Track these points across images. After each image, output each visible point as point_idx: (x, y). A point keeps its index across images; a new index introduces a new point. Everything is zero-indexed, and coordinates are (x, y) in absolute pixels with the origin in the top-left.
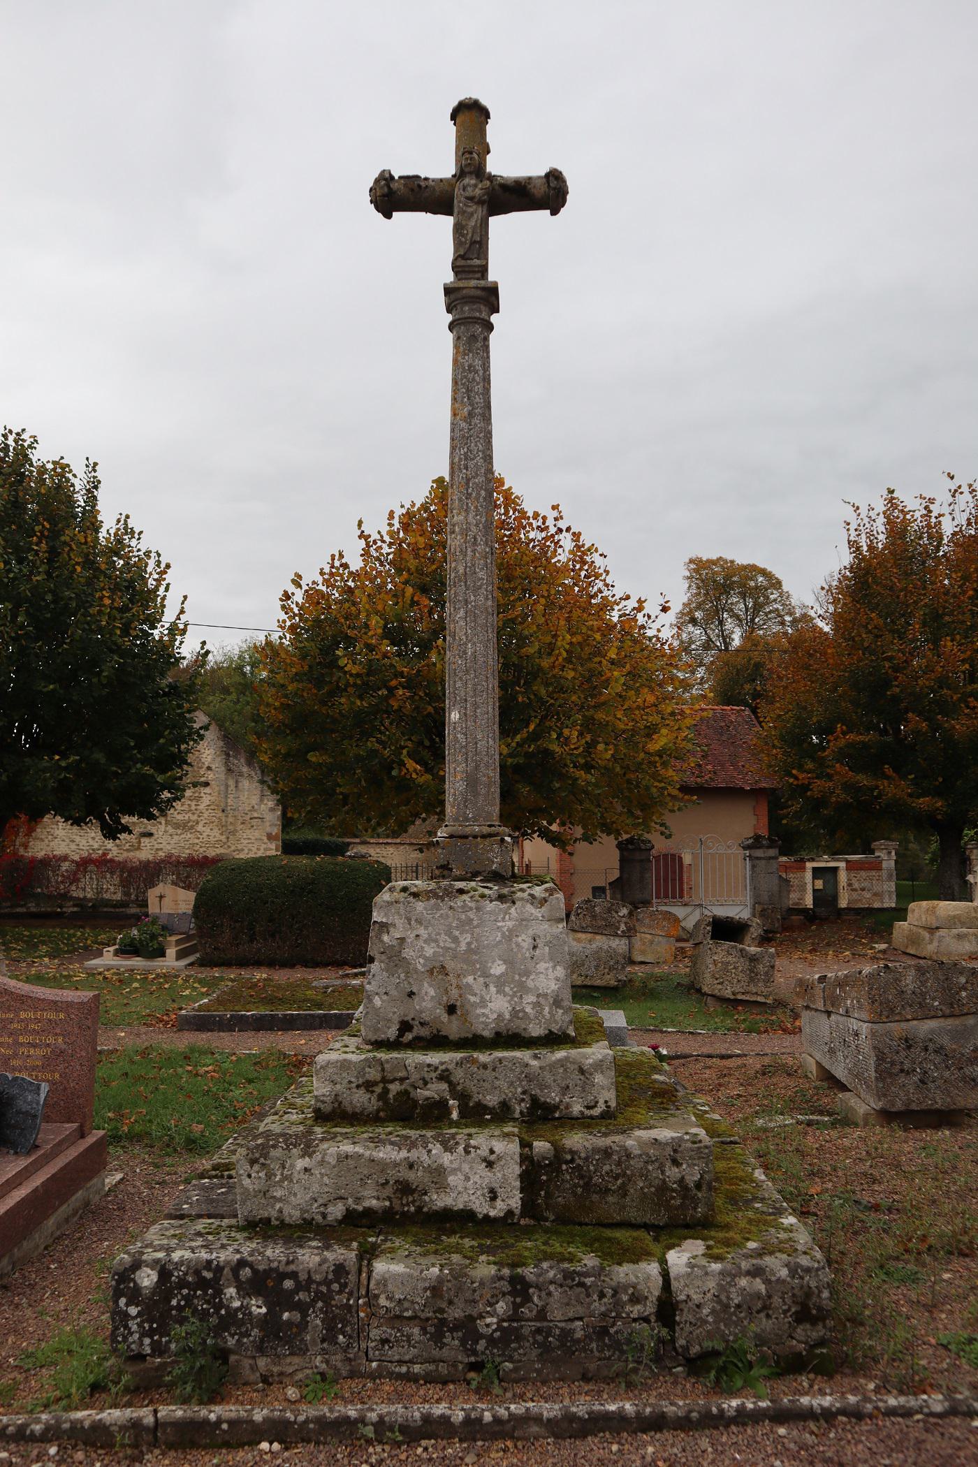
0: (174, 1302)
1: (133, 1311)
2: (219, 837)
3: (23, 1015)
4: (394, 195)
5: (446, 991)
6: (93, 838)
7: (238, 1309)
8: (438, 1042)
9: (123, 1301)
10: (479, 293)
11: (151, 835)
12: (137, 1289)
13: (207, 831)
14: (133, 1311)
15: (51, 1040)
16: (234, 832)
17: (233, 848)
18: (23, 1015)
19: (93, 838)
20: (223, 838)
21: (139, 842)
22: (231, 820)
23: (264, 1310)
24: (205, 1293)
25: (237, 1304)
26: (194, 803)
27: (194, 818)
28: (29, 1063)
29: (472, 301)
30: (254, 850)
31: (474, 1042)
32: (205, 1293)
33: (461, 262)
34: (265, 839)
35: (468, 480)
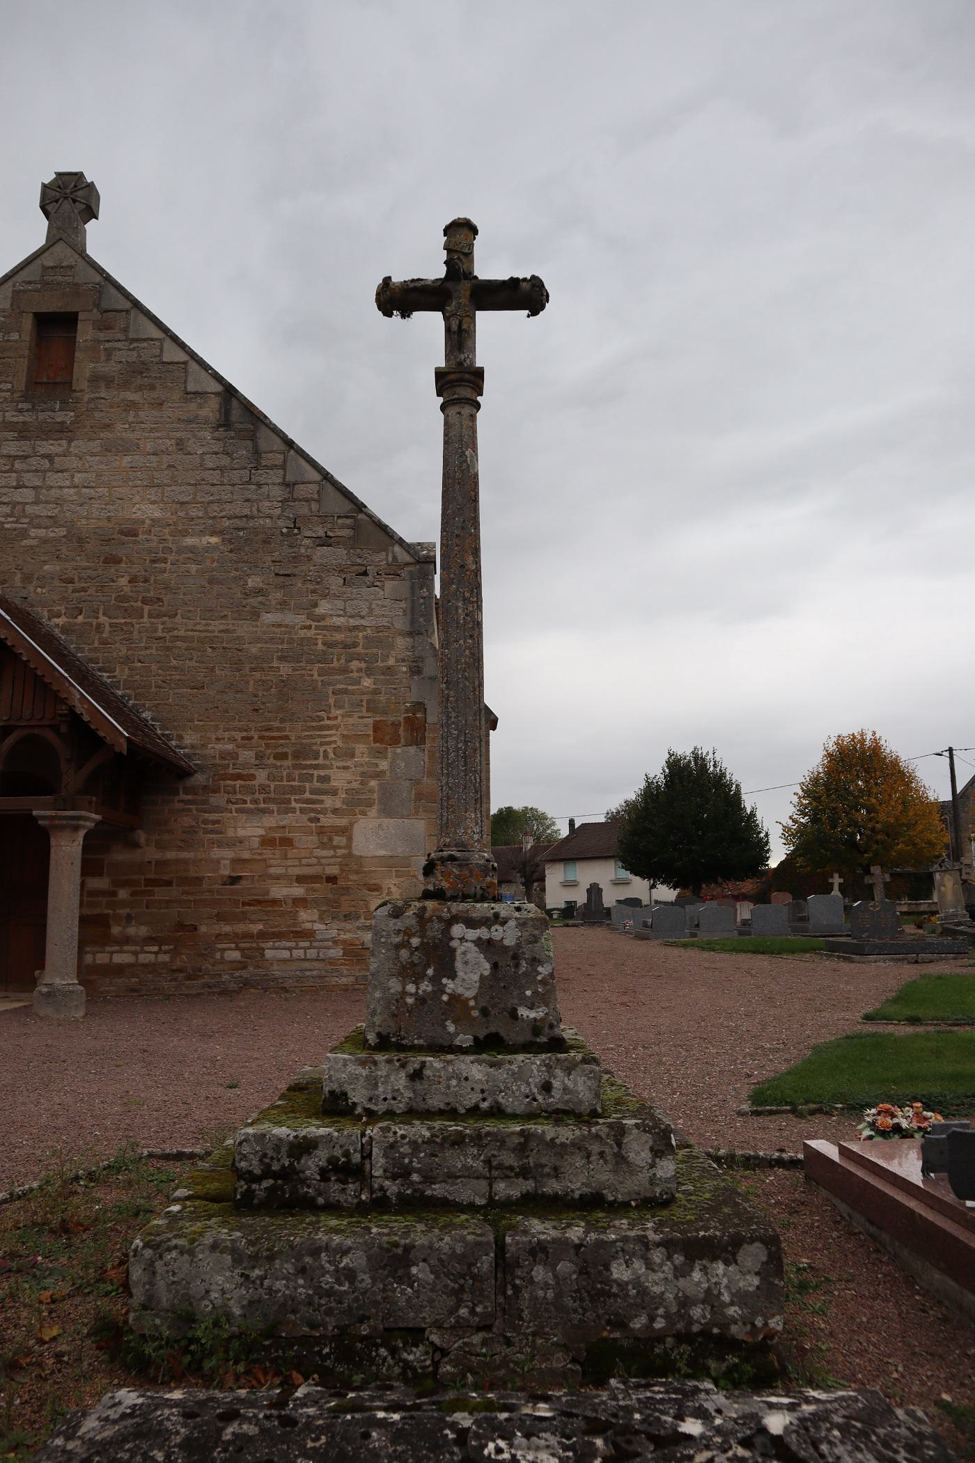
29: (460, 383)
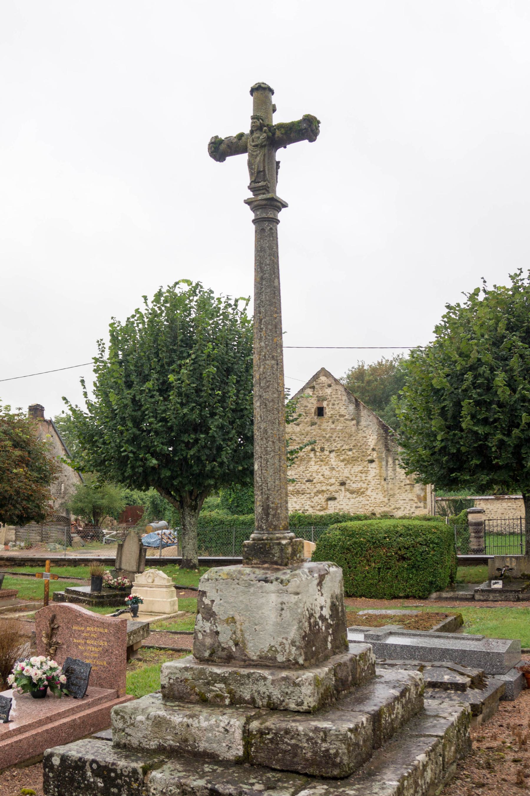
0: (67, 774)
1: (51, 775)
2: (383, 499)
3: (88, 629)
4: (220, 149)
5: (234, 633)
6: (296, 502)
7: (92, 782)
8: (229, 659)
9: (47, 770)
10: (264, 202)
11: (334, 499)
12: (52, 765)
13: (374, 495)
14: (51, 775)
15: (102, 643)
16: (393, 495)
17: (393, 507)
18: (88, 629)
19: (296, 502)
20: (386, 500)
21: (327, 504)
22: (390, 486)
23: (102, 785)
24: (79, 773)
25: (92, 780)
26: (364, 475)
27: (365, 486)
28: (92, 655)
29: (266, 207)
30: (408, 508)
31: (248, 663)
32: (79, 773)
33: (253, 185)
34: (416, 499)
35: (261, 320)
